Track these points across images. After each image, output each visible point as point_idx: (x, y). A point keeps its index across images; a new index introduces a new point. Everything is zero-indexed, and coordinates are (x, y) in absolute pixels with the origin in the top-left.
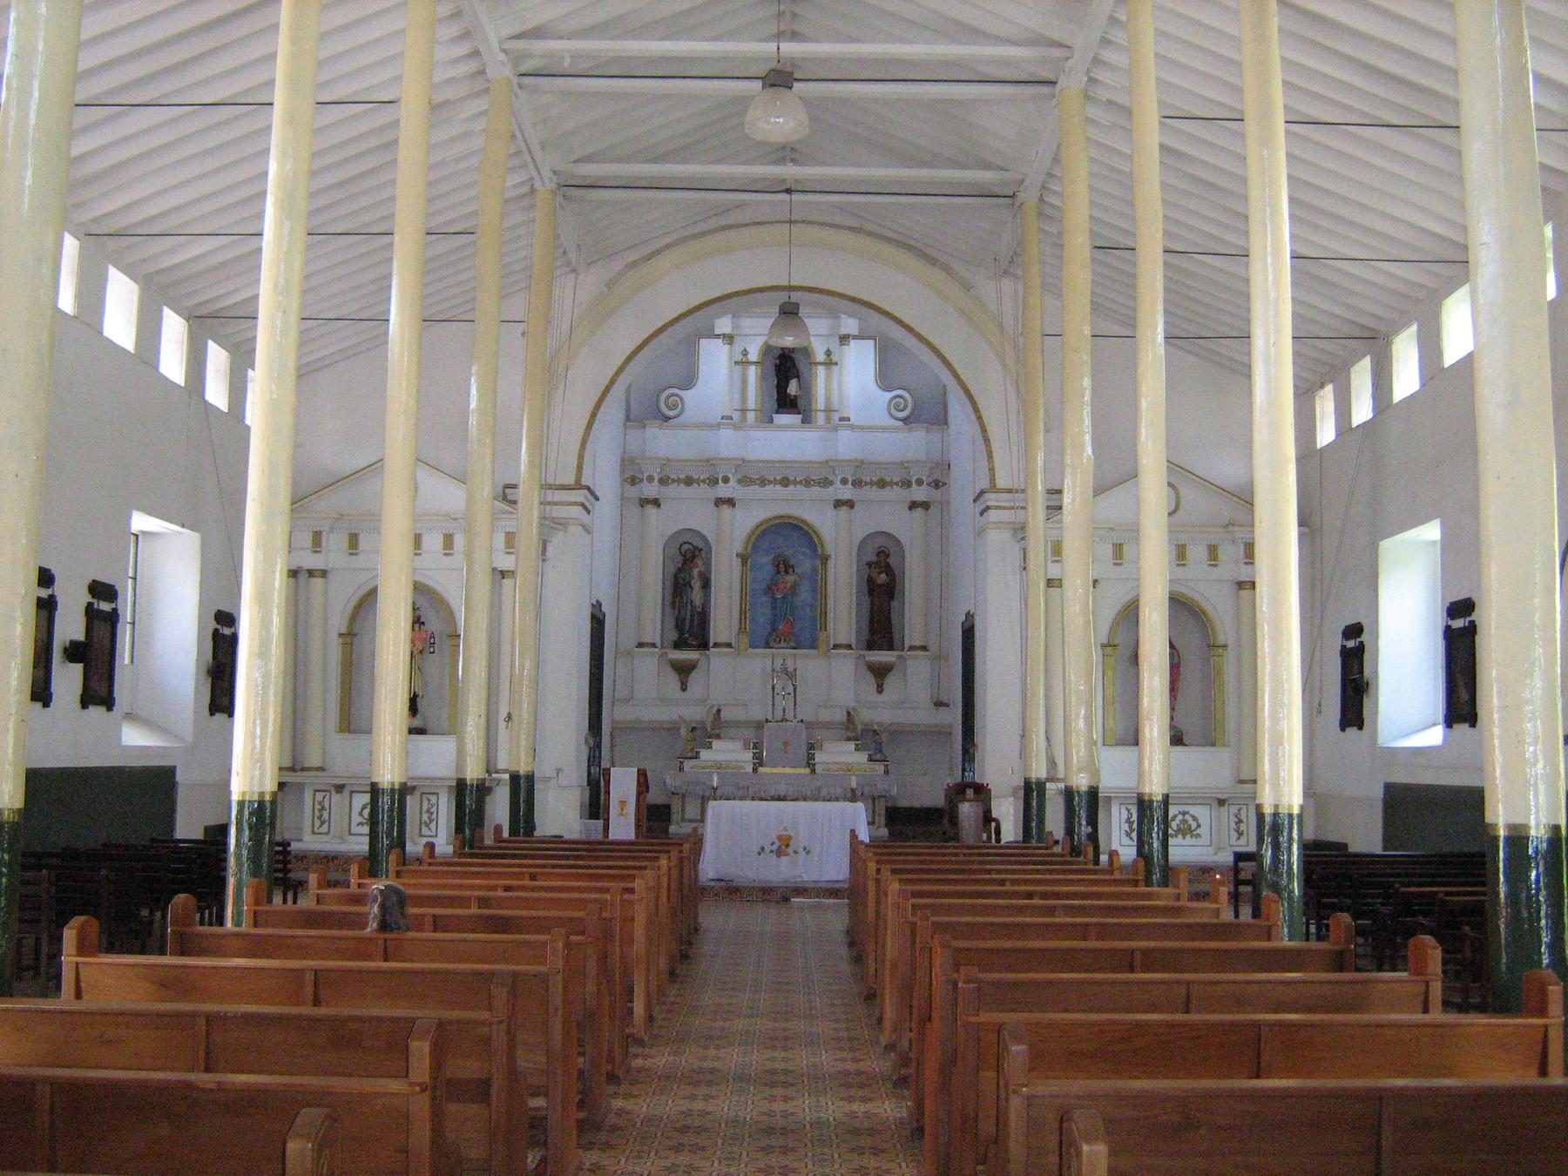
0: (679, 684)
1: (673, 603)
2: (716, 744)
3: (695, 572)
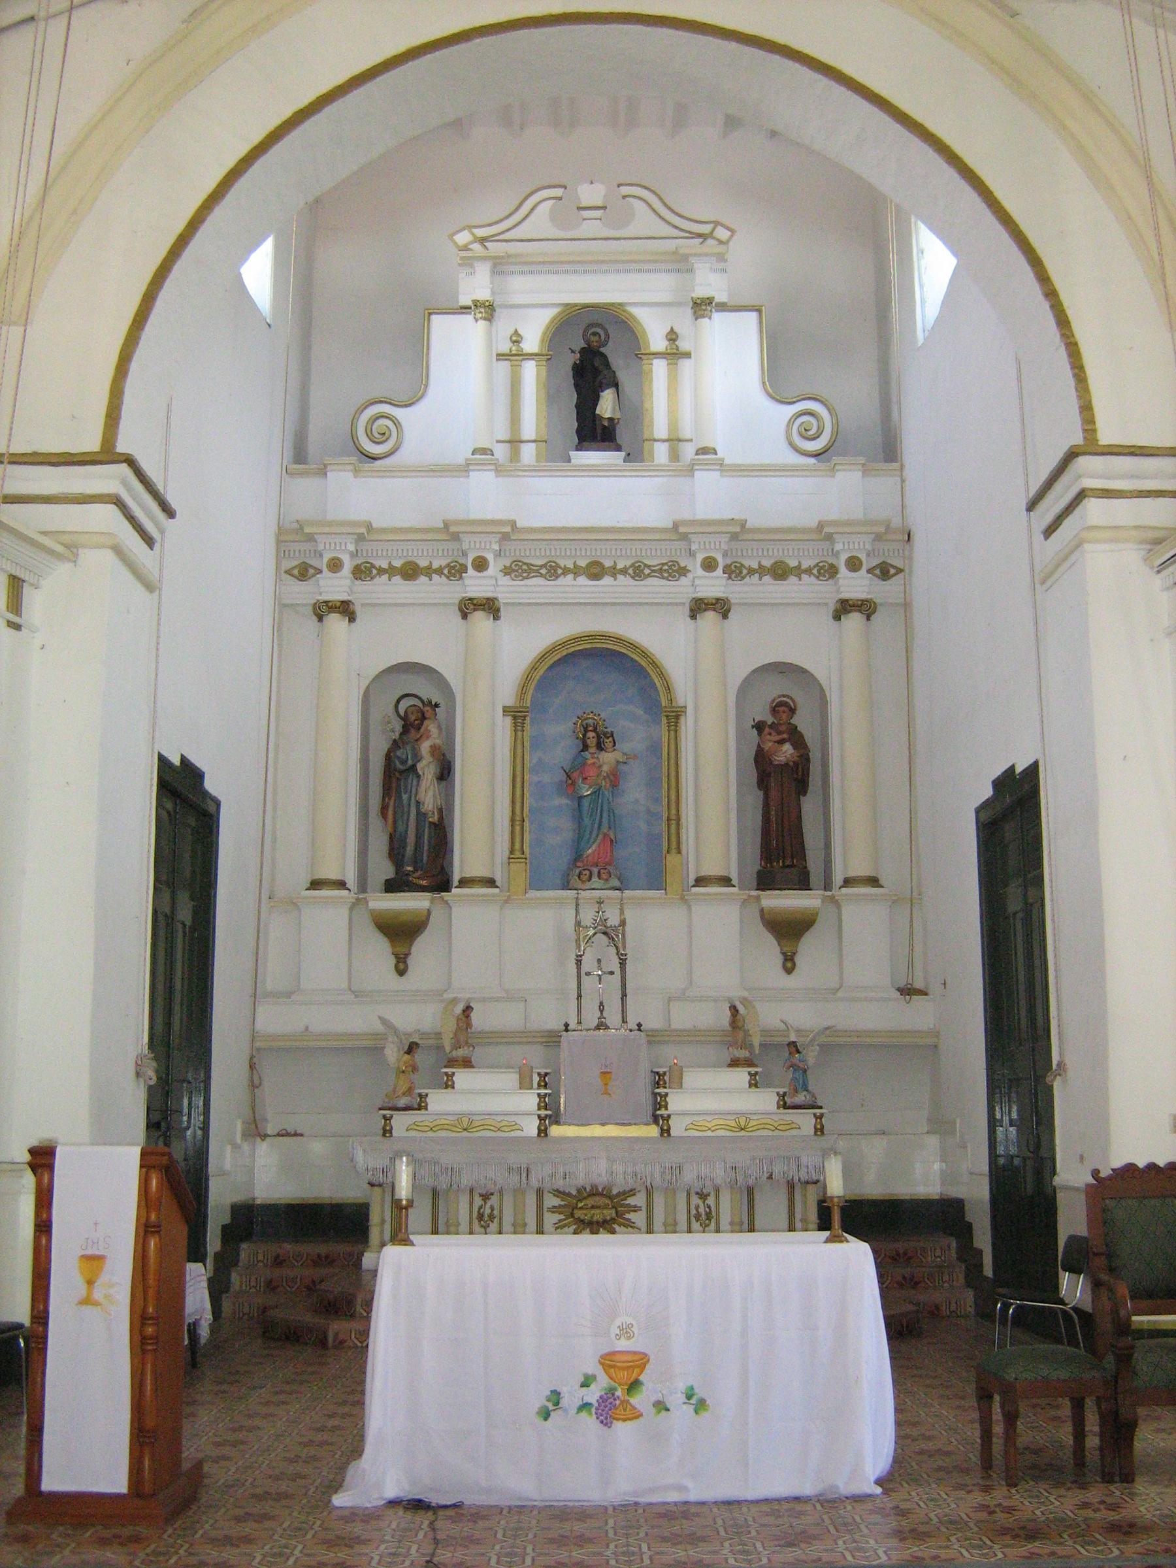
0: (392, 961)
1: (384, 809)
2: (462, 1078)
3: (425, 747)
